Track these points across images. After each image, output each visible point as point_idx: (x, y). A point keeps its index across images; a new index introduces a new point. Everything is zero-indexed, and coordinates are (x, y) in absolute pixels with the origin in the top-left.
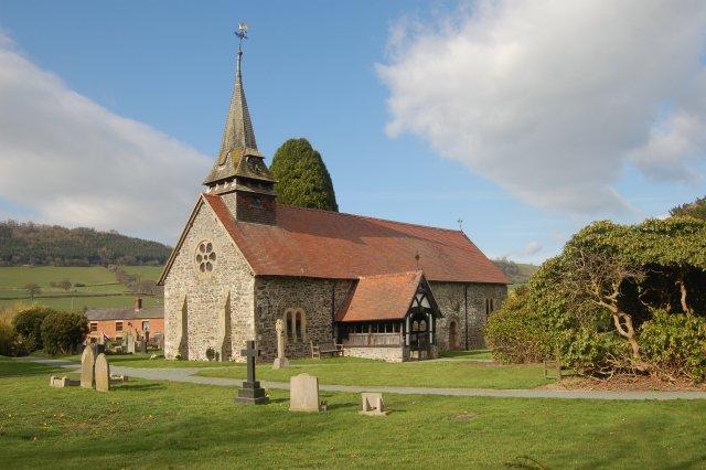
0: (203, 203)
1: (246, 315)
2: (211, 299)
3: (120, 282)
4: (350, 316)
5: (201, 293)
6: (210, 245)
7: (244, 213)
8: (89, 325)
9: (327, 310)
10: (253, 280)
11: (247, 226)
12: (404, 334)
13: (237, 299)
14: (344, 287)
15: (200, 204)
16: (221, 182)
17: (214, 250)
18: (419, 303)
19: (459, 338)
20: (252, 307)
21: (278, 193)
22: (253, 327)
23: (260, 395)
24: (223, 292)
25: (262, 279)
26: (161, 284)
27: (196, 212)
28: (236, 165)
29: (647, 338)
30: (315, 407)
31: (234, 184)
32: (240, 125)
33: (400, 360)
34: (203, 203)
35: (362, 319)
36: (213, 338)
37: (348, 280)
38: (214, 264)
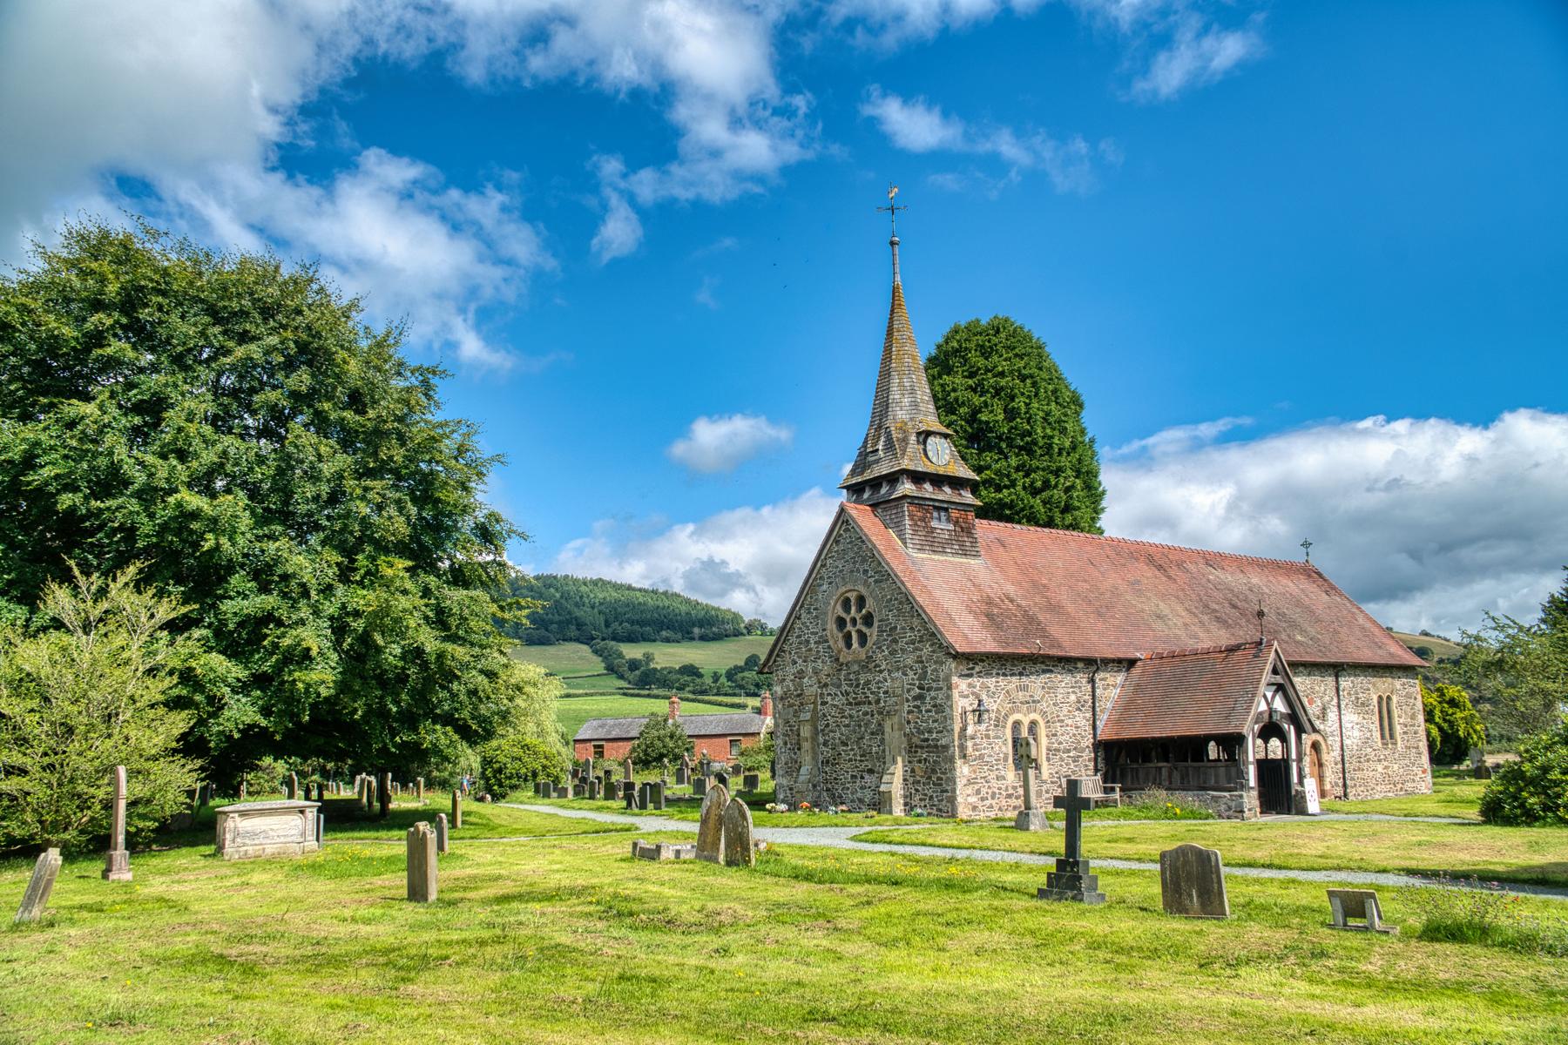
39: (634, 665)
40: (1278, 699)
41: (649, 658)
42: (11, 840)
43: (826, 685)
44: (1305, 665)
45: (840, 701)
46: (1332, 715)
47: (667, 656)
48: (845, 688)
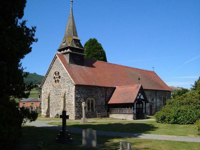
9: (103, 99)
10: (74, 87)
11: (75, 67)
13: (68, 94)
15: (56, 58)
16: (63, 49)
18: (140, 97)
20: (74, 97)
22: (74, 105)
24: (63, 91)
28: (69, 43)
31: (68, 50)
32: (71, 28)
33: (132, 119)
34: (57, 57)
35: (121, 102)
38: (60, 80)
43: (51, 91)
46: (155, 100)
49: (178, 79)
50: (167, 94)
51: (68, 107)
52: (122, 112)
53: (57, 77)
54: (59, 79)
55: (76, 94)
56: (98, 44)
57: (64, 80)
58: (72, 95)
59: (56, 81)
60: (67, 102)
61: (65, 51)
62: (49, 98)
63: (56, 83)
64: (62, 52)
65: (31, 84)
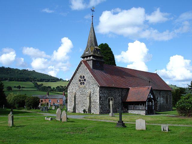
0: (82, 63)
1: (96, 98)
2: (86, 94)
3: (35, 87)
4: (129, 99)
5: (80, 92)
6: (84, 76)
7: (95, 67)
8: (40, 101)
9: (120, 98)
10: (99, 88)
11: (95, 71)
12: (146, 106)
13: (93, 94)
14: (125, 91)
15: (81, 63)
16: (87, 57)
17: (85, 78)
18: (150, 96)
19: (158, 108)
20: (98, 96)
21: (101, 58)
22: (98, 103)
23: (124, 125)
24: (88, 91)
25: (101, 88)
26: (67, 88)
27: (79, 66)
28: (92, 52)
29: (56, 109)
30: (144, 129)
31: (91, 58)
32: (93, 39)
33: (145, 114)
34: (82, 63)
35: (132, 101)
36: (84, 106)
37: (126, 88)
38: (85, 82)
39: (40, 86)
40: (152, 95)
41: (42, 85)
42: (185, 111)
43: (77, 91)
44: (155, 90)
45: (79, 94)
46: (159, 98)
47: (46, 84)
48: (80, 92)
49: (177, 72)
50: (169, 94)
51: (93, 104)
52: (136, 108)
53: (82, 80)
54: (84, 82)
55: (100, 93)
56: (109, 48)
57: (89, 82)
58: (96, 95)
59: (81, 83)
60: (92, 101)
61: (88, 58)
62: (75, 97)
63: (81, 85)
64: (85, 59)
65: (2, 78)
